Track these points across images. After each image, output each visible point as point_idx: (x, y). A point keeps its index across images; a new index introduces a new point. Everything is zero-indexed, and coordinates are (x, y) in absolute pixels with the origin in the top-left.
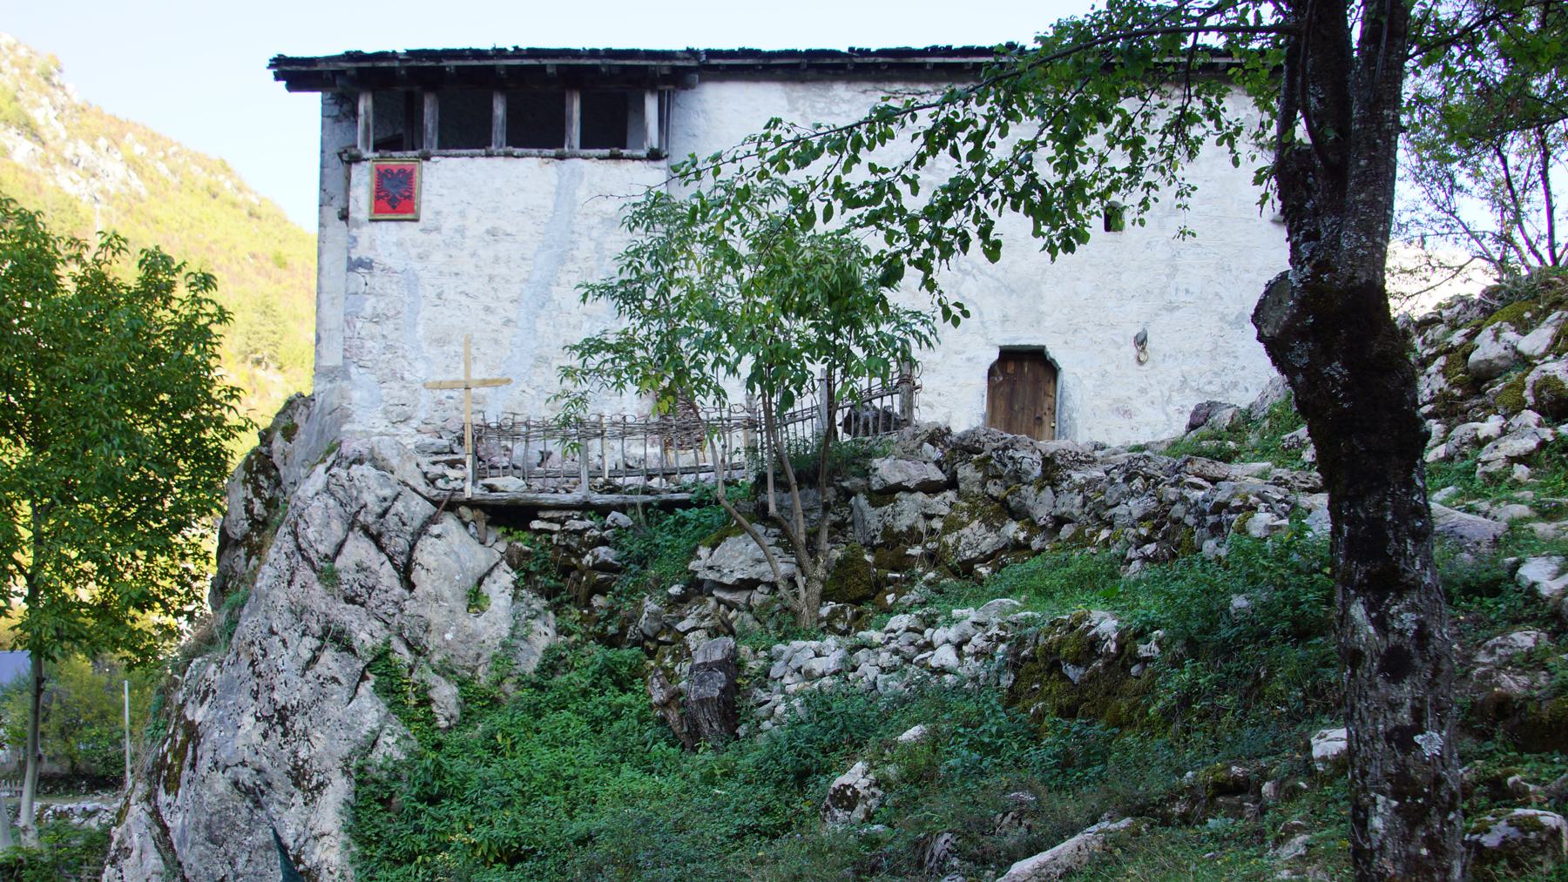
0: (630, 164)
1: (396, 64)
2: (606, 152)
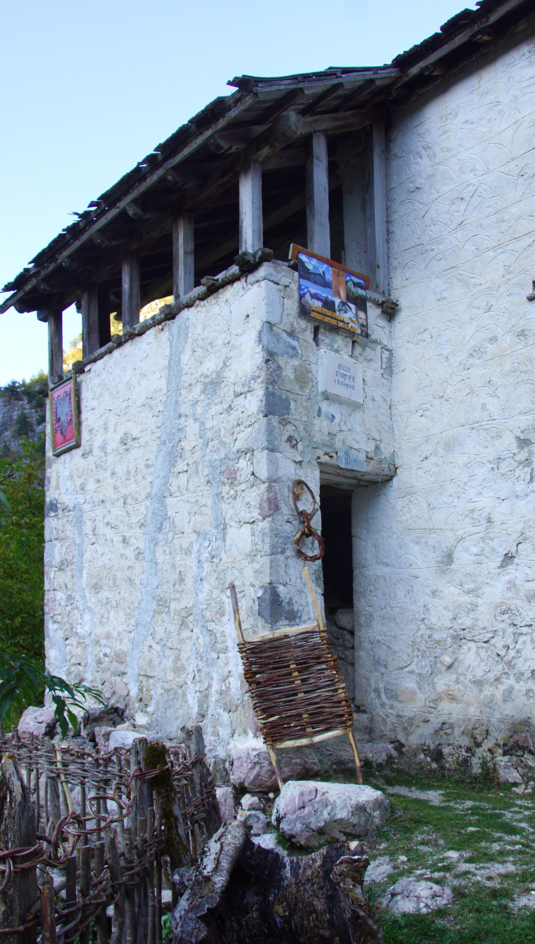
0: (229, 292)
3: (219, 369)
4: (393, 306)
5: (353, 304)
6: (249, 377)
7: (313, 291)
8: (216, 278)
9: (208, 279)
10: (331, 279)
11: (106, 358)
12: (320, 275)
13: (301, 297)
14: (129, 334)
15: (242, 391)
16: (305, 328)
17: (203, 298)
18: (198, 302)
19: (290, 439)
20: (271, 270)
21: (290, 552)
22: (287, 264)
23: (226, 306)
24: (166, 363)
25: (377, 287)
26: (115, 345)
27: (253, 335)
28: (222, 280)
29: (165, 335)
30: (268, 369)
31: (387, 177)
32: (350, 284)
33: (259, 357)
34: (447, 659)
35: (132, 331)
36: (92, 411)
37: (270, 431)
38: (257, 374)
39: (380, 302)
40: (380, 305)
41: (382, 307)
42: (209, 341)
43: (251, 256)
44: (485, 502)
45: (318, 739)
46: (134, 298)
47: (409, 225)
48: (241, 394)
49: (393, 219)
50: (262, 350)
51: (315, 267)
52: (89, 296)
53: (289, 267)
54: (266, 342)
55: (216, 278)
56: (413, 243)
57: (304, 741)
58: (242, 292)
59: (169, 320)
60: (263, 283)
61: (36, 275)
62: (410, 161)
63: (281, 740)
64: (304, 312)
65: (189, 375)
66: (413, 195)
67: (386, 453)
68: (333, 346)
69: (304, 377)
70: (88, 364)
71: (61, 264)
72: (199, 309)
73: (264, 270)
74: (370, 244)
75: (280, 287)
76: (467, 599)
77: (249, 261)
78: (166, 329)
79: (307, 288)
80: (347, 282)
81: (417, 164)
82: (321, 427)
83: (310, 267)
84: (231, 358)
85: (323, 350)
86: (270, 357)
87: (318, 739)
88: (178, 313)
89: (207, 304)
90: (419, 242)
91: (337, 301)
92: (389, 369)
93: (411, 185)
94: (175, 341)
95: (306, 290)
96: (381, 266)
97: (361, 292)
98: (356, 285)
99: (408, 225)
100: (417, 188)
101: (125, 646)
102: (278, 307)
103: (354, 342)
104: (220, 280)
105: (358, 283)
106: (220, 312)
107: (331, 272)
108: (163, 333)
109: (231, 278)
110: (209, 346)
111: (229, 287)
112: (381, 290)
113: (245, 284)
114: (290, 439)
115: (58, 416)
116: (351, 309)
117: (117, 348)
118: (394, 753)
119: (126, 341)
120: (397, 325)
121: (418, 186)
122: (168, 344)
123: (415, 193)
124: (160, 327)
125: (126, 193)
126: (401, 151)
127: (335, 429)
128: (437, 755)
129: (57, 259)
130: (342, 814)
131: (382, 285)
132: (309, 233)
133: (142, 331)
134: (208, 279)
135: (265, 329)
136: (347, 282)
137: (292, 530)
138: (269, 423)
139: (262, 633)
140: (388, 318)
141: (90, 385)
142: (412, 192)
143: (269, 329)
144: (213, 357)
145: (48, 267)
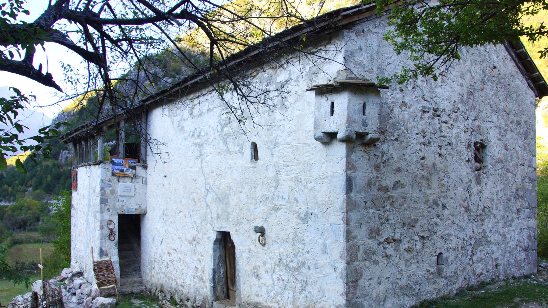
7: (116, 168)
16: (115, 179)
19: (108, 209)
21: (107, 238)
32: (130, 163)
34: (153, 266)
37: (101, 208)
44: (158, 226)
45: (109, 287)
57: (106, 287)
63: (101, 286)
67: (143, 207)
69: (113, 192)
76: (156, 251)
82: (119, 205)
83: (116, 162)
85: (121, 183)
86: (102, 189)
87: (109, 287)
91: (125, 169)
92: (145, 183)
97: (134, 164)
98: (132, 163)
101: (83, 254)
114: (108, 209)
118: (144, 290)
127: (124, 203)
128: (150, 292)
130: (98, 306)
137: (108, 232)
138: (101, 206)
139: (97, 259)
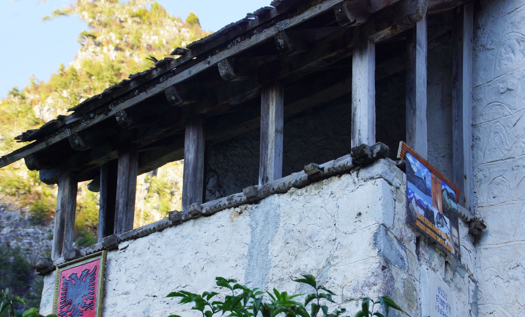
0: (336, 184)
1: (67, 133)
2: (302, 175)
3: (321, 267)
4: (481, 227)
5: (448, 217)
6: (361, 282)
7: (418, 197)
8: (321, 166)
9: (314, 167)
10: (431, 186)
11: (152, 236)
12: (422, 179)
13: (409, 201)
14: (195, 212)
15: (353, 296)
17: (300, 185)
18: (293, 189)
20: (386, 168)
22: (395, 162)
23: (331, 199)
24: (245, 251)
25: (465, 201)
26: (171, 223)
27: (368, 236)
28: (329, 169)
29: (244, 220)
30: (385, 277)
31: (474, 71)
33: (374, 263)
35: (199, 210)
36: (124, 296)
38: (372, 280)
39: (469, 220)
40: (468, 223)
41: (469, 227)
42: (308, 234)
43: (369, 150)
46: (199, 172)
47: (496, 133)
48: (351, 300)
49: (478, 122)
50: (378, 255)
51: (419, 171)
52: (131, 160)
53: (398, 166)
54: (382, 246)
55: (321, 166)
56: (502, 155)
58: (352, 187)
59: (251, 203)
60: (379, 181)
61: (71, 126)
62: (501, 55)
64: (411, 220)
65: (279, 269)
66: (502, 97)
68: (431, 264)
70: (124, 240)
71: (114, 117)
72: (294, 196)
73: (380, 167)
74: (457, 150)
75: (393, 188)
77: (367, 155)
78: (245, 213)
79: (413, 193)
80: (443, 191)
81: (509, 59)
84: (337, 257)
88: (264, 198)
89: (306, 194)
90: (509, 155)
91: (436, 212)
93: (501, 85)
94: (259, 228)
95: (412, 195)
96: (468, 177)
99: (496, 133)
100: (509, 90)
102: (392, 210)
103: (446, 263)
104: (326, 170)
105: (451, 194)
106: (323, 205)
107: (430, 178)
108: (241, 217)
109: (340, 169)
110: (307, 242)
111: (335, 179)
112: (468, 205)
113: (356, 179)
115: (68, 299)
116: (446, 223)
117: (171, 226)
119: (187, 220)
120: (482, 251)
121: (510, 87)
122: (249, 230)
123: (504, 95)
124: (238, 210)
125: (223, 47)
126: (490, 42)
129: (110, 110)
131: (468, 199)
132: (409, 130)
133: (211, 211)
134: (314, 167)
135: (382, 232)
136: (443, 191)
140: (473, 241)
141: (123, 265)
142: (502, 93)
143: (385, 233)
144: (313, 252)
145: (94, 118)
